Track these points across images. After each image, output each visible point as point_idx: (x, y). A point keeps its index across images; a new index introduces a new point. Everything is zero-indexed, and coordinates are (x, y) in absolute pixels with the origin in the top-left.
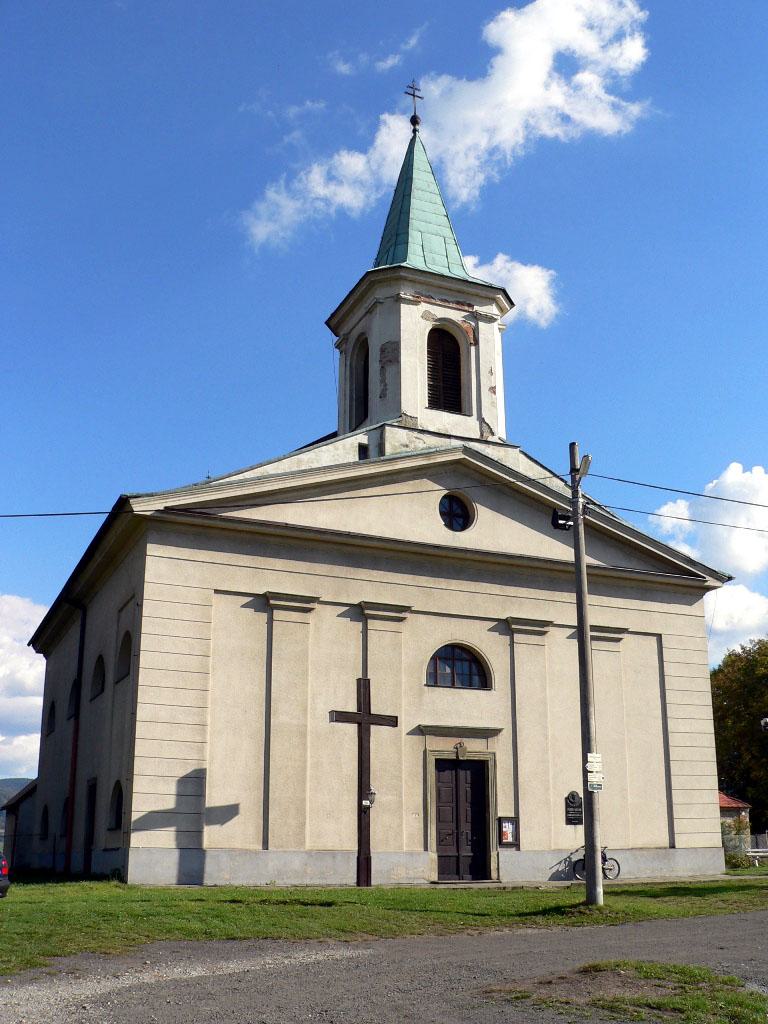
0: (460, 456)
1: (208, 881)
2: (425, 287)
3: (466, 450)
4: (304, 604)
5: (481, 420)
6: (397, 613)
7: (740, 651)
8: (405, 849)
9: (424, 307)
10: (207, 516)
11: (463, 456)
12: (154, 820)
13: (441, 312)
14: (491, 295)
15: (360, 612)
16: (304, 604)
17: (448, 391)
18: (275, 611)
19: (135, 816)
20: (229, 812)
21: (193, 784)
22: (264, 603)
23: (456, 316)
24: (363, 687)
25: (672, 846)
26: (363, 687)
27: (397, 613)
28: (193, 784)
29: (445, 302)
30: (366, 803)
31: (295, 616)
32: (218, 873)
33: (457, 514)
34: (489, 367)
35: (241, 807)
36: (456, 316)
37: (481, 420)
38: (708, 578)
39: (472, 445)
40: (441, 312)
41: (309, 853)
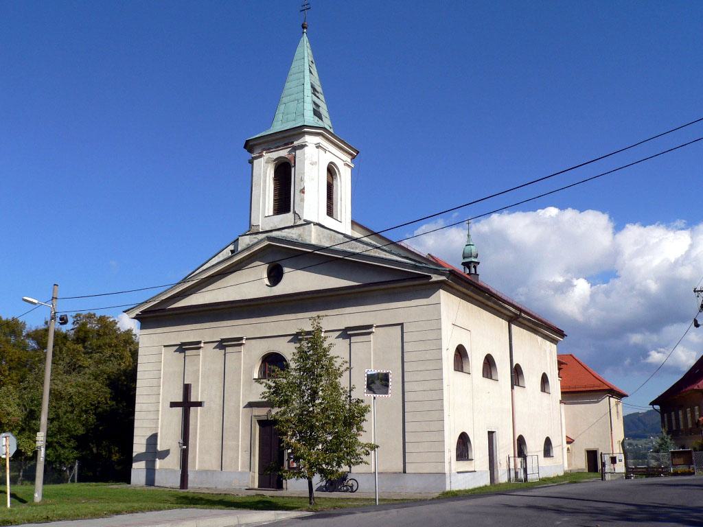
0: (267, 243)
1: (156, 484)
2: (266, 144)
3: (269, 239)
4: (196, 346)
5: (295, 213)
6: (237, 342)
7: (325, 345)
8: (240, 470)
9: (266, 156)
10: (164, 310)
11: (269, 243)
12: (140, 457)
13: (275, 155)
14: (299, 131)
15: (222, 344)
16: (196, 346)
17: (283, 203)
18: (227, 348)
19: (134, 454)
20: (165, 454)
21: (153, 440)
22: (182, 348)
23: (284, 153)
24: (187, 389)
25: (405, 472)
26: (187, 389)
27: (237, 342)
28: (153, 440)
29: (277, 148)
30: (185, 447)
31: (194, 352)
32: (160, 479)
33: (275, 276)
34: (300, 177)
35: (171, 452)
36: (284, 153)
37: (295, 213)
38: (432, 275)
39: (274, 234)
40: (275, 155)
41: (197, 472)
